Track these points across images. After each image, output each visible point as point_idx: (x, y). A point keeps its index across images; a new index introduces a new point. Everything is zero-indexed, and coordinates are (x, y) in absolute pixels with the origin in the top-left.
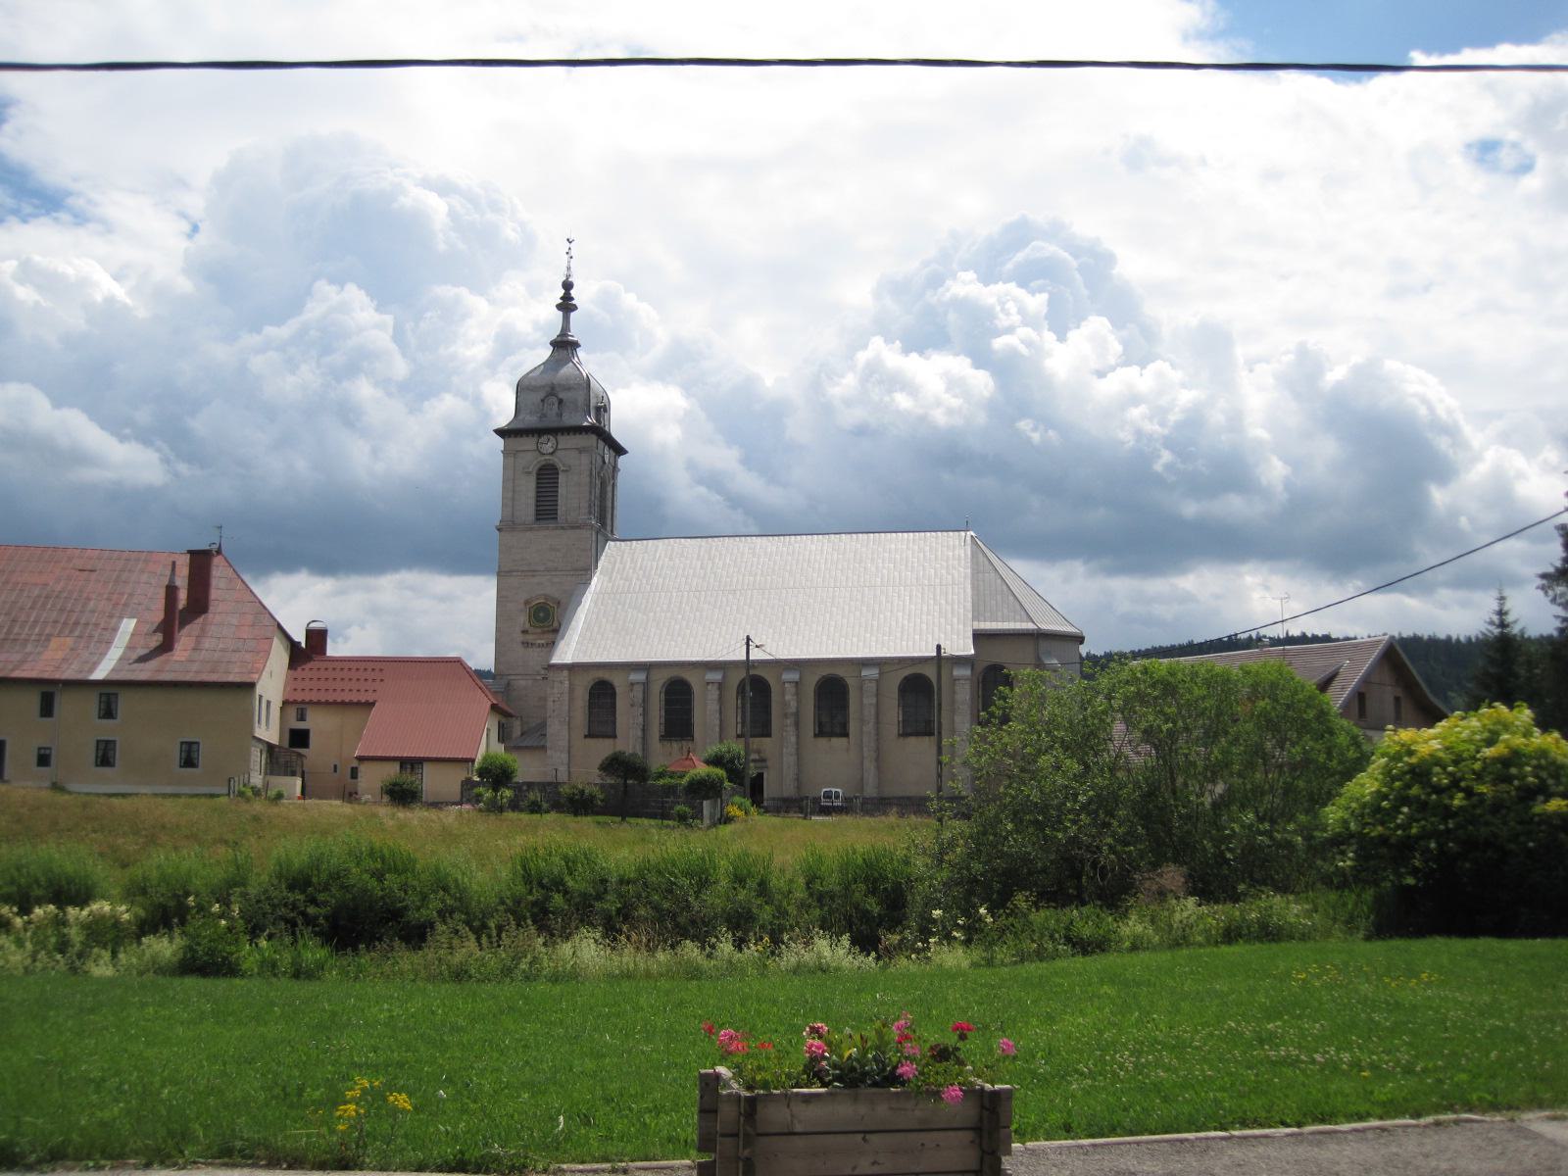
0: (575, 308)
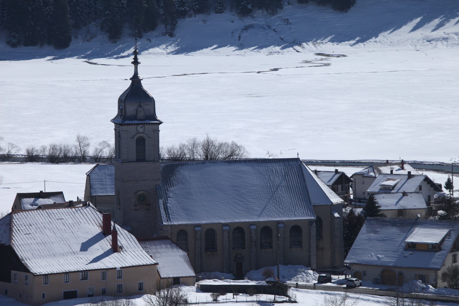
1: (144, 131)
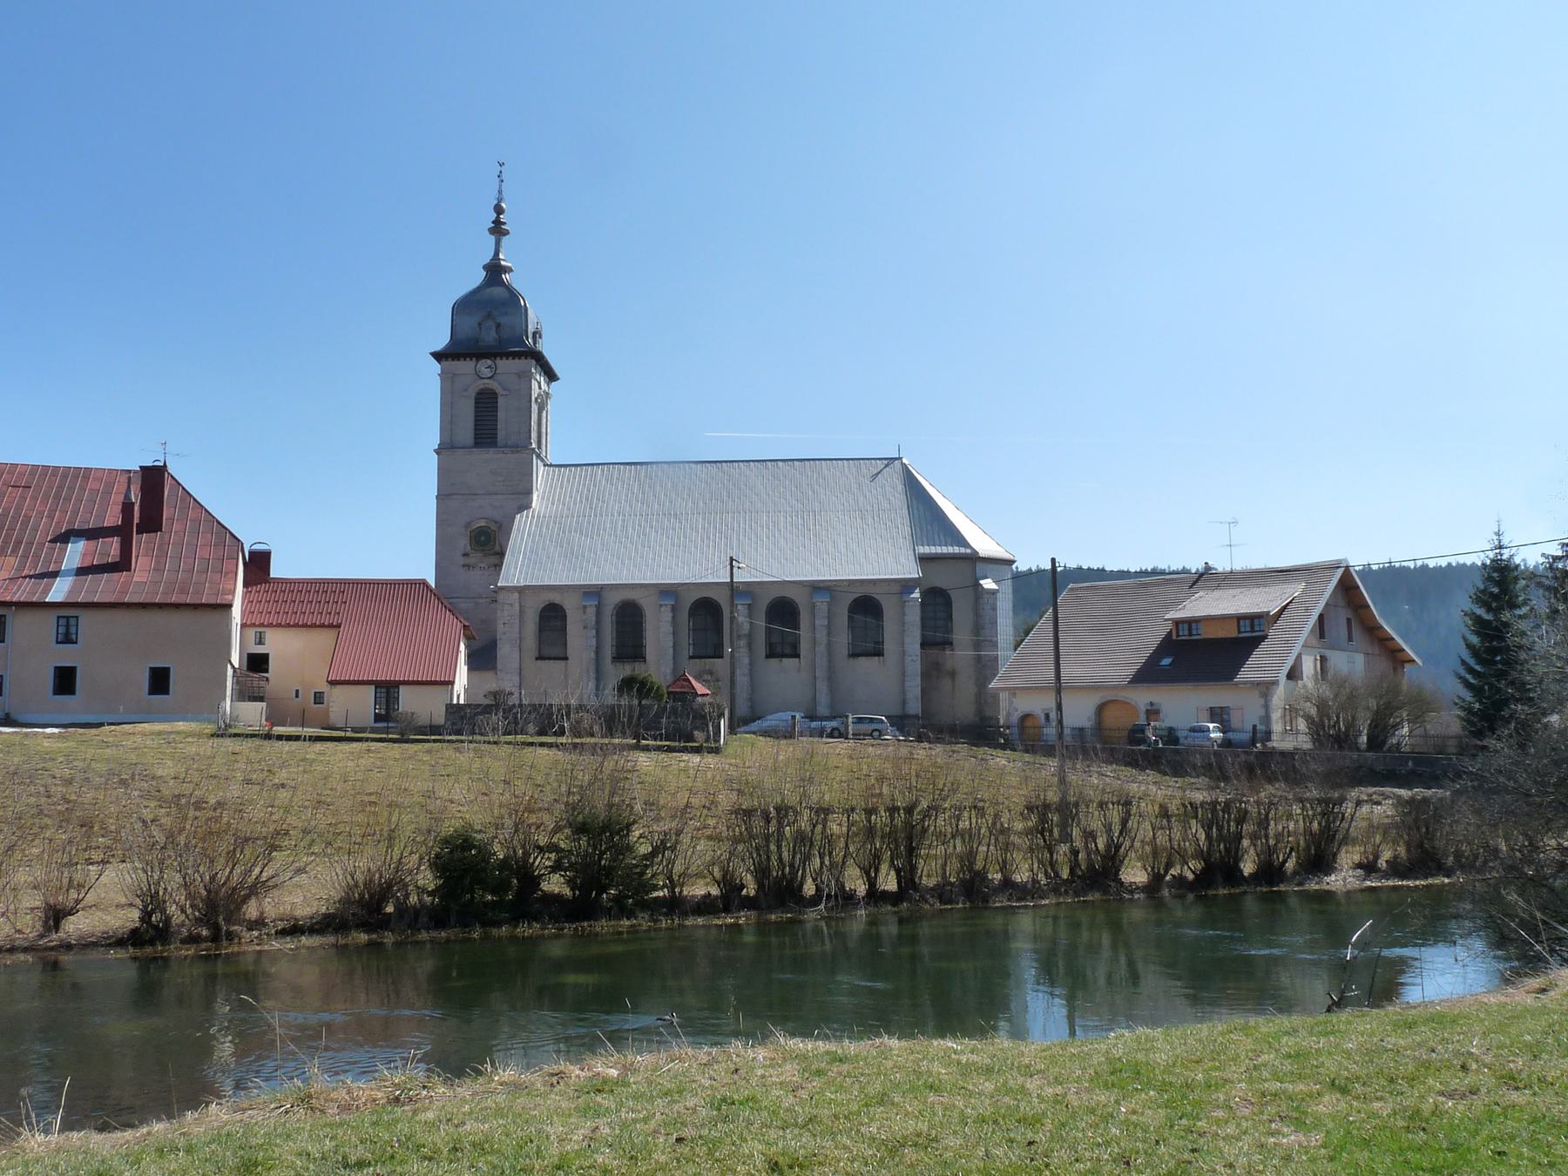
0: (506, 233)
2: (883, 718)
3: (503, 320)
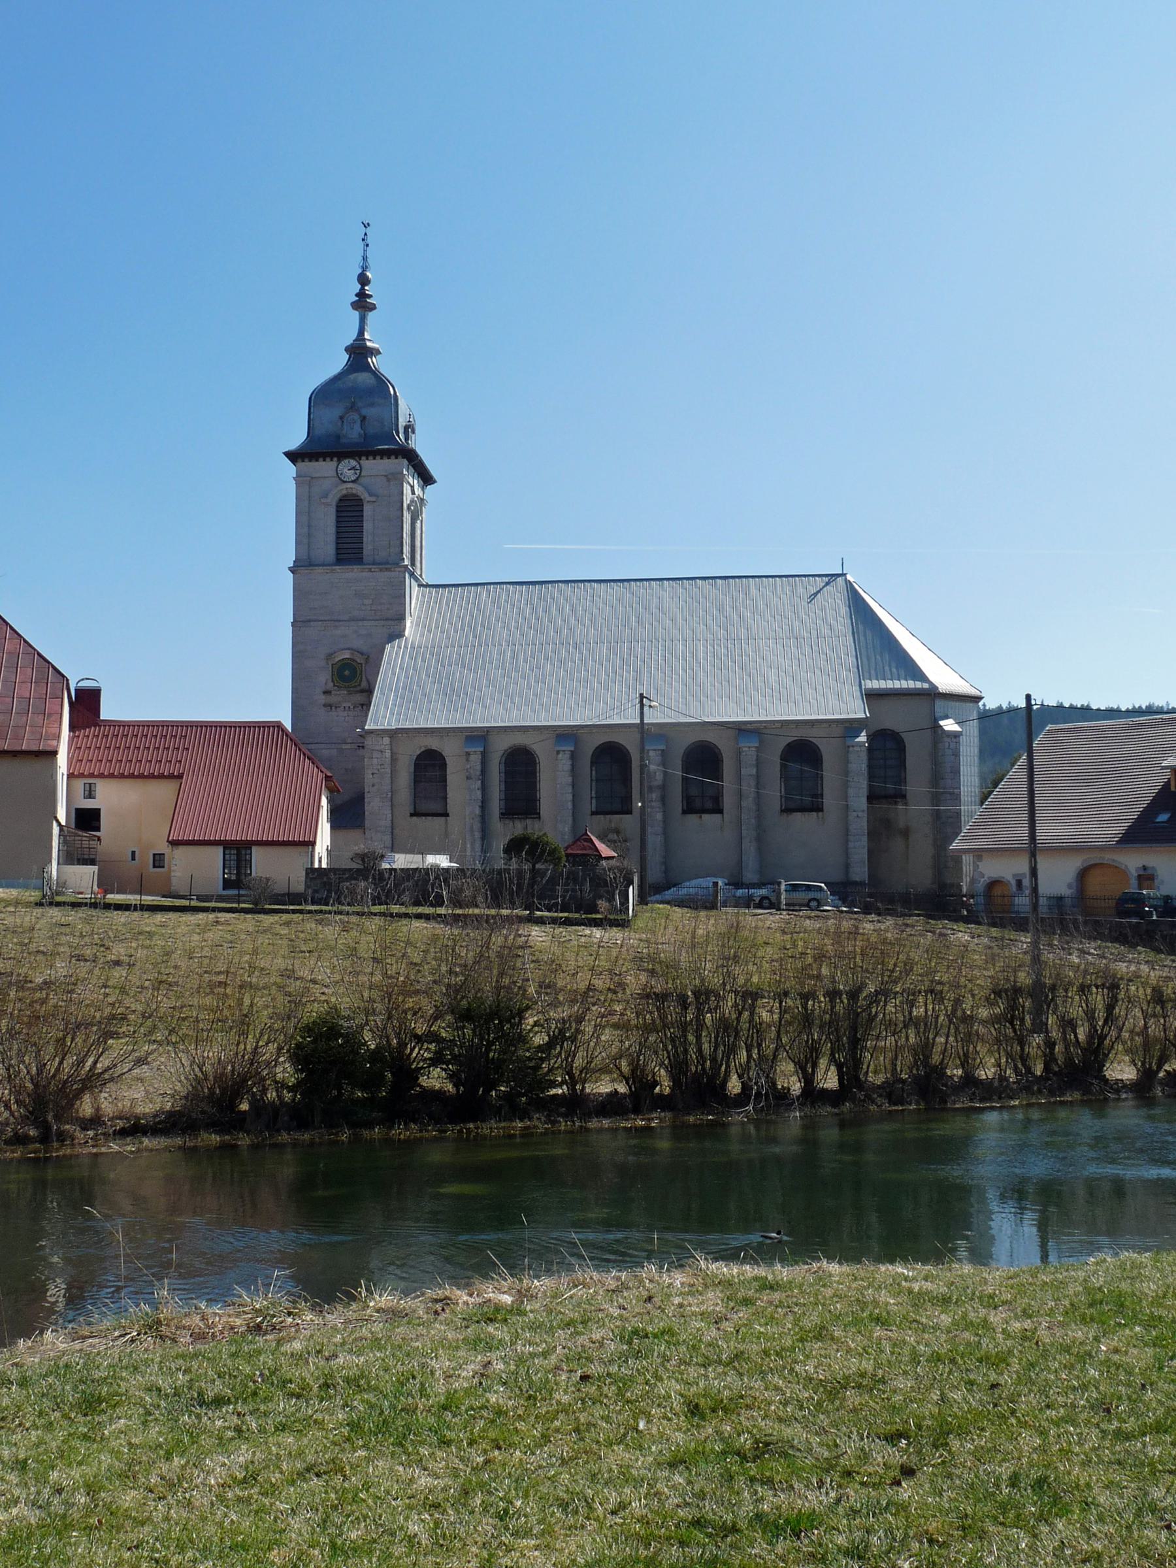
0: (373, 307)
1: (361, 470)
2: (823, 885)
3: (369, 412)
